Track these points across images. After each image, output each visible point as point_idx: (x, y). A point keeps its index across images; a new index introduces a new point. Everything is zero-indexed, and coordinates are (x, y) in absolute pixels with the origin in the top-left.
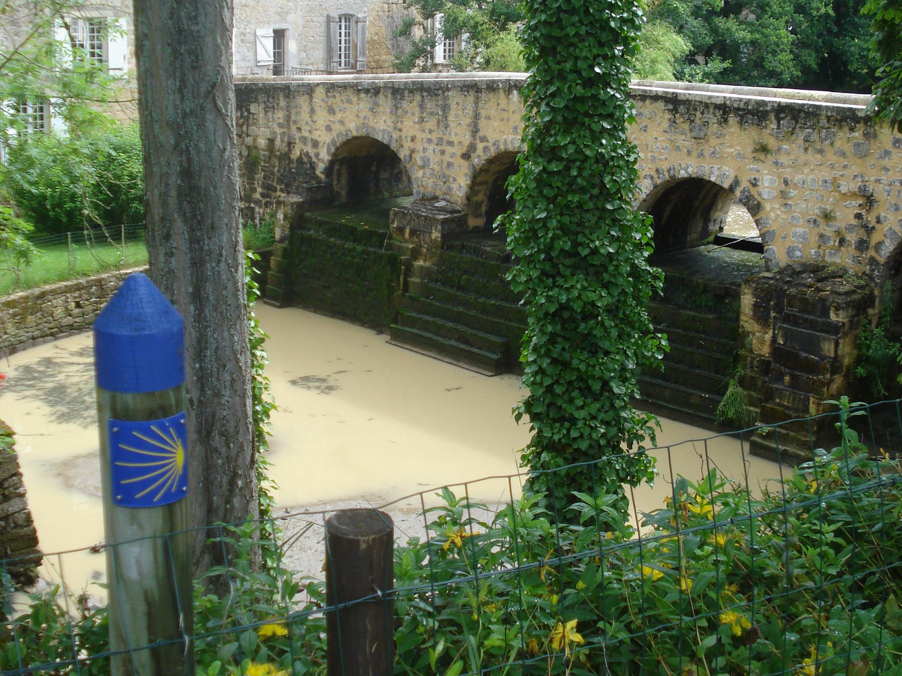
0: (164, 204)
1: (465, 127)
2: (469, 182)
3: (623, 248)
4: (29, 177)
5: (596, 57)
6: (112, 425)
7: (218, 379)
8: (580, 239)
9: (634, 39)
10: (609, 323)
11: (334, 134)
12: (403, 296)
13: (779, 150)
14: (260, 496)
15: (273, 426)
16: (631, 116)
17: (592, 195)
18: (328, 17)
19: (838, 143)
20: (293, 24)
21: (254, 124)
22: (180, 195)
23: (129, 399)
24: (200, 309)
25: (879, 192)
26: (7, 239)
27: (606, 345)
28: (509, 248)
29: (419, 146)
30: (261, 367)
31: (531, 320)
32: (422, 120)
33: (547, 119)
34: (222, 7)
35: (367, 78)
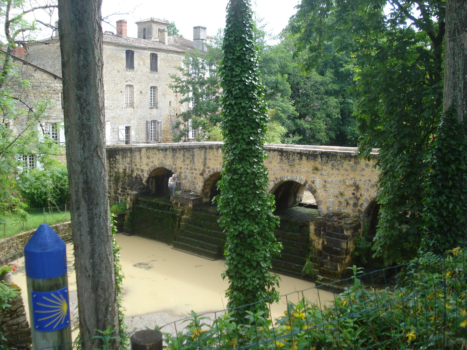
0: (77, 195)
1: (201, 163)
2: (203, 184)
3: (264, 208)
4: (25, 186)
5: (251, 133)
6: (33, 294)
7: (100, 266)
8: (247, 205)
9: (265, 126)
10: (259, 239)
11: (150, 166)
12: (178, 230)
13: (322, 169)
14: (118, 314)
15: (123, 284)
16: (265, 156)
17: (251, 188)
18: (147, 121)
19: (344, 166)
20: (133, 125)
21: (118, 163)
22: (83, 190)
23: (40, 281)
24: (92, 238)
25: (361, 184)
26: (17, 211)
27: (257, 247)
28: (218, 210)
29: (183, 171)
30: (118, 261)
31: (228, 238)
32: (184, 161)
33: (232, 158)
34: (100, 115)
35: (162, 145)
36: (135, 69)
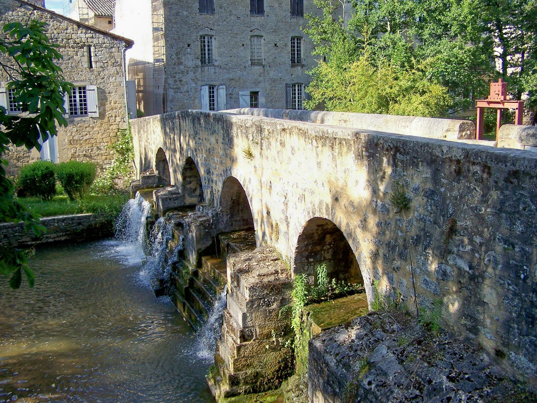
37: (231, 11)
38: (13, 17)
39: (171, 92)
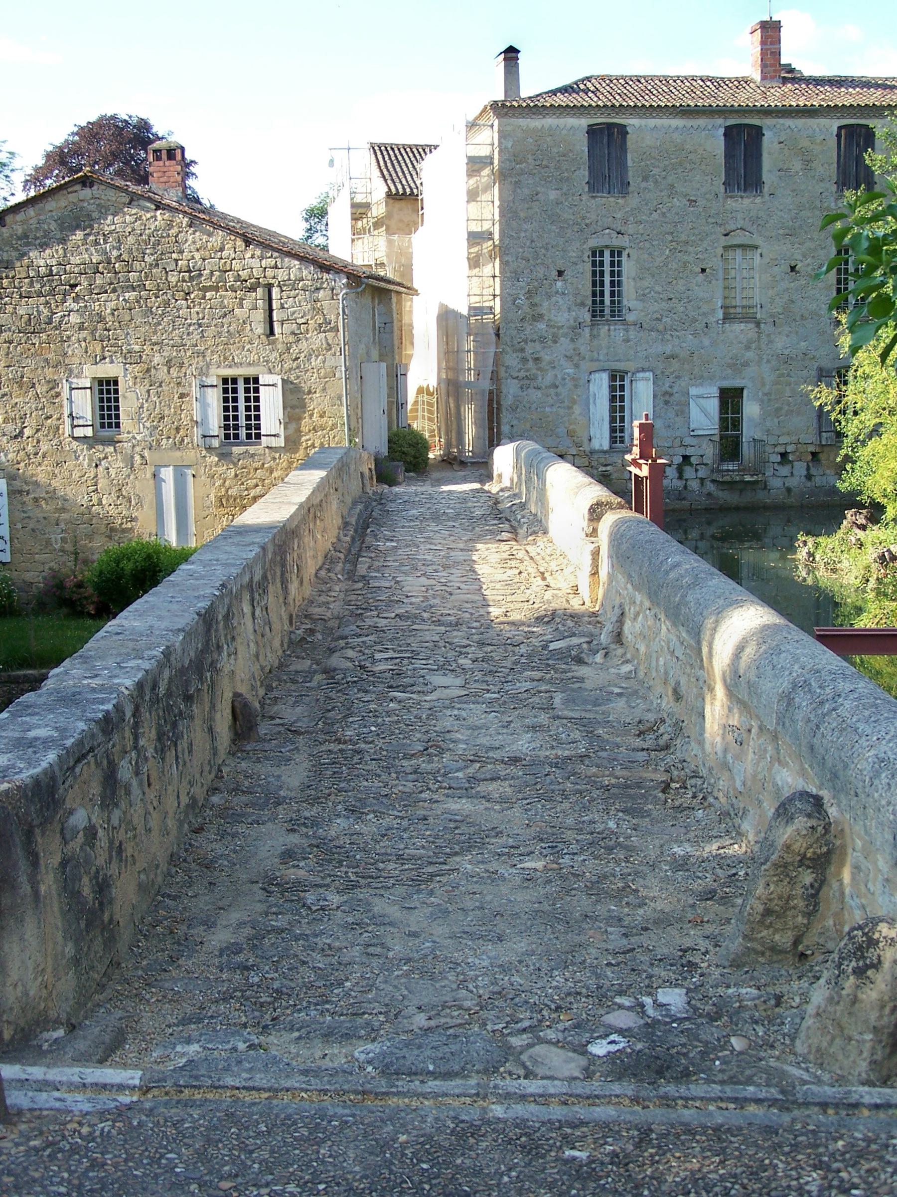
36: (766, 189)
37: (672, 186)
38: (113, 227)
39: (511, 389)
